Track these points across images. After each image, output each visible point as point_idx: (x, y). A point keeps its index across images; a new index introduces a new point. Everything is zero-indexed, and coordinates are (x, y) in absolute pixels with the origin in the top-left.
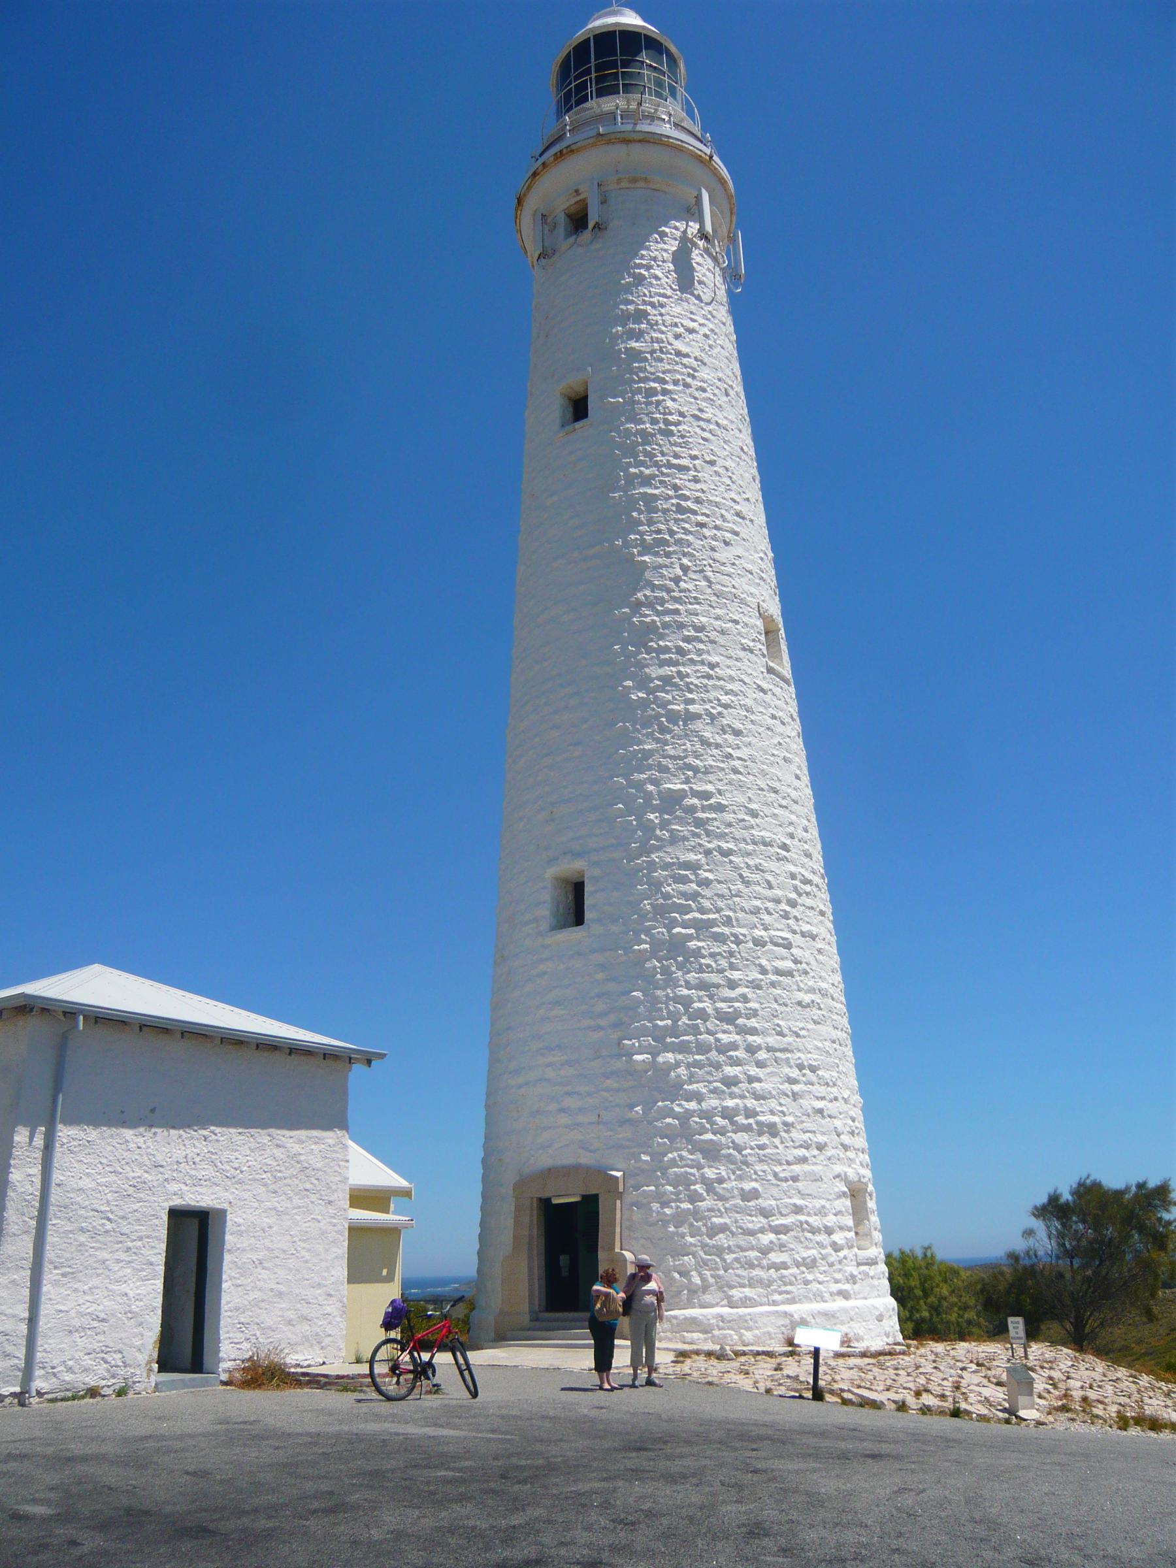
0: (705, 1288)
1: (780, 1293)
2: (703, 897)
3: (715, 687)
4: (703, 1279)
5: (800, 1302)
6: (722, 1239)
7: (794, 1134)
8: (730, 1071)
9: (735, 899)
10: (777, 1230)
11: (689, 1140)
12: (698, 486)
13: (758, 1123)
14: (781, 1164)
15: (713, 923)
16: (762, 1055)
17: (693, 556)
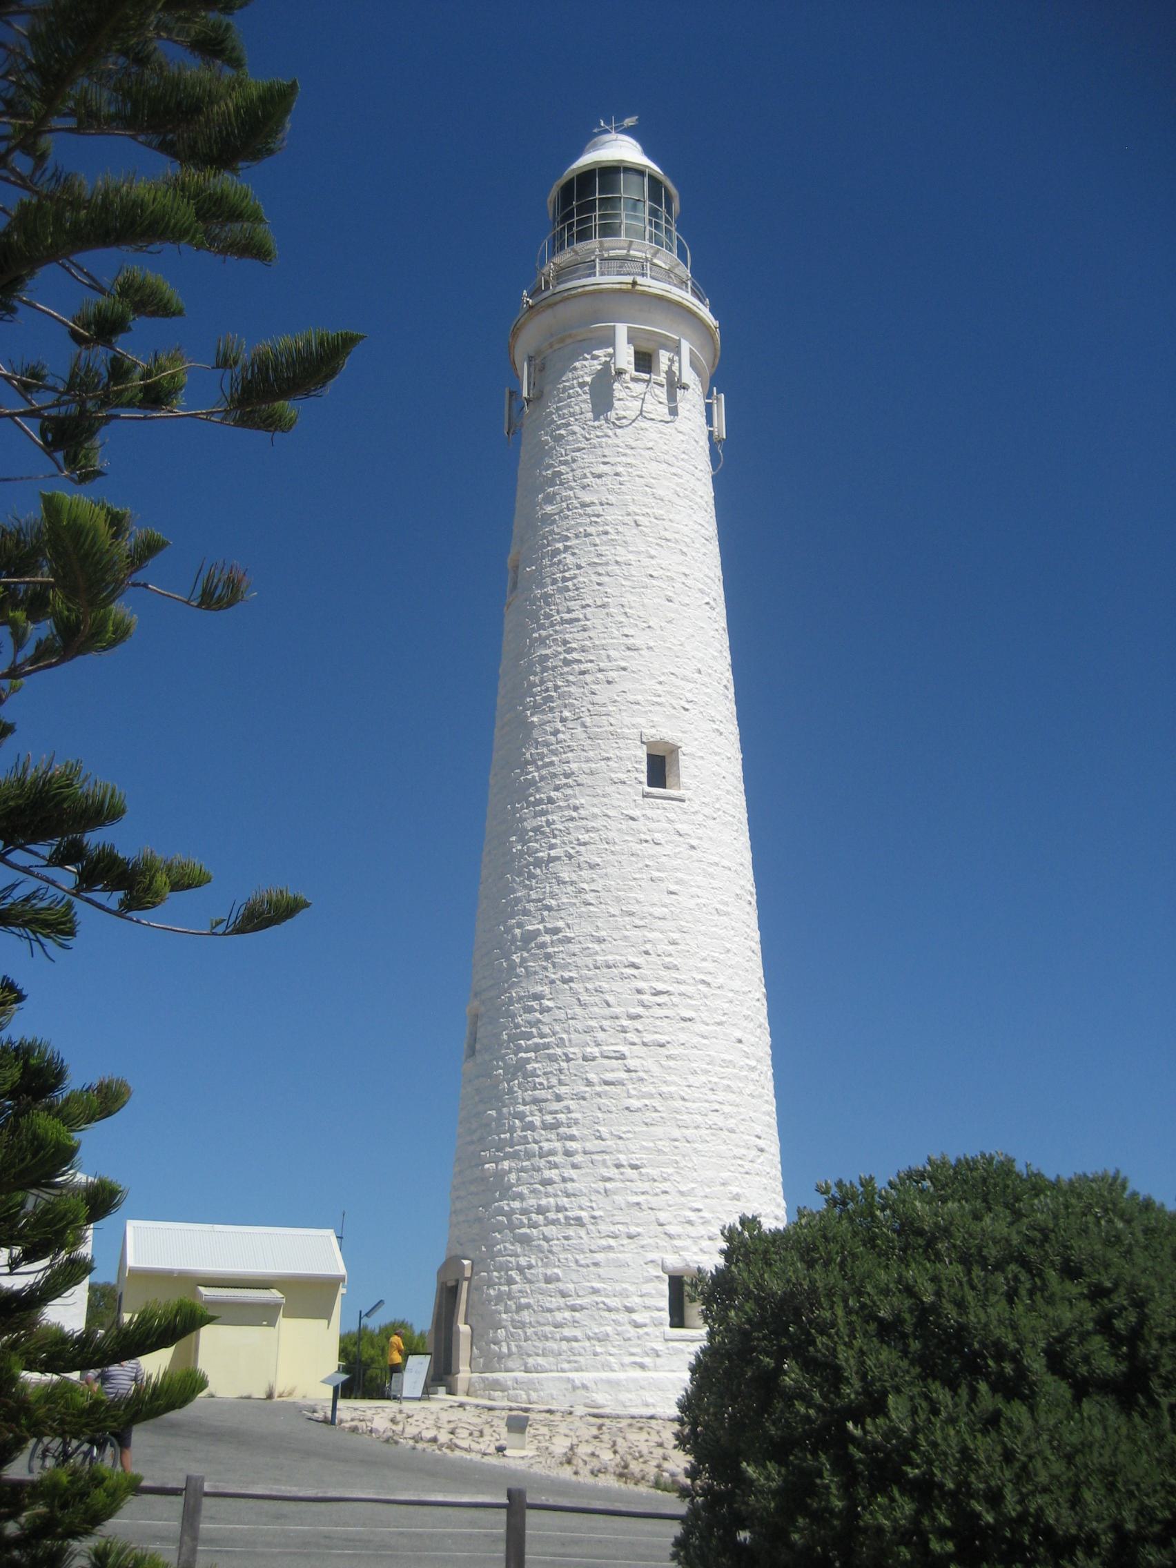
0: (510, 1354)
1: (569, 1362)
2: (543, 1023)
3: (577, 828)
4: (509, 1349)
5: (587, 1370)
6: (526, 1316)
7: (603, 1227)
8: (547, 1174)
9: (571, 1022)
10: (573, 1309)
11: (512, 1231)
12: (586, 634)
13: (566, 1218)
14: (584, 1253)
15: (547, 1046)
16: (578, 1159)
17: (573, 705)
